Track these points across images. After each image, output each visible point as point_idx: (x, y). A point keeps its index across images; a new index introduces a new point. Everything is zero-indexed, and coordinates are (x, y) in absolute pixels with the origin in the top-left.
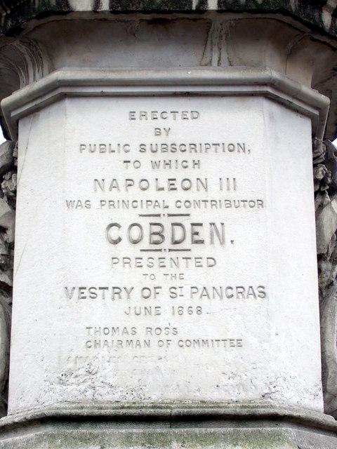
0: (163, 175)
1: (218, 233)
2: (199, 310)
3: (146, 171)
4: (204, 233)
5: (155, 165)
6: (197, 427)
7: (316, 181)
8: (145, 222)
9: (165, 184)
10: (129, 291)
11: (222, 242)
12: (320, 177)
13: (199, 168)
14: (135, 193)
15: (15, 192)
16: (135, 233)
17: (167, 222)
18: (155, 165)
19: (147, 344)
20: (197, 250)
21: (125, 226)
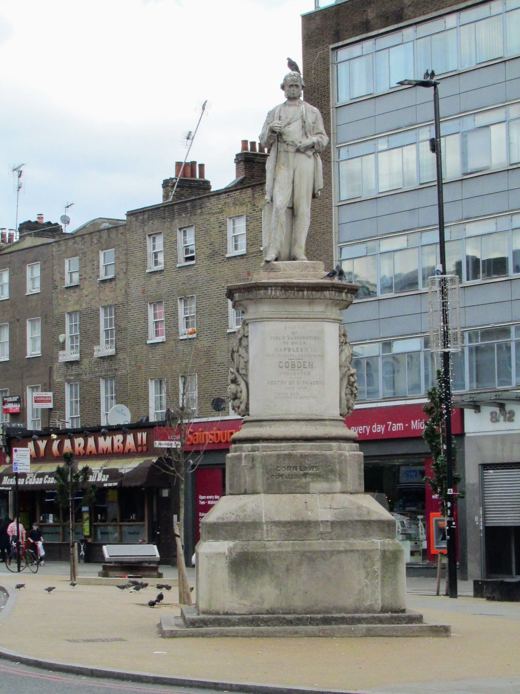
0: (292, 352)
1: (311, 366)
2: (305, 388)
3: (290, 346)
4: (307, 365)
5: (293, 343)
6: (344, 285)
7: (340, 342)
8: (290, 361)
9: (295, 349)
10: (285, 382)
11: (312, 367)
12: (341, 341)
13: (427, 70)
14: (287, 352)
15: (247, 346)
16: (287, 365)
17: (296, 361)
18: (293, 343)
19: (291, 398)
20: (305, 370)
21: (284, 363)
